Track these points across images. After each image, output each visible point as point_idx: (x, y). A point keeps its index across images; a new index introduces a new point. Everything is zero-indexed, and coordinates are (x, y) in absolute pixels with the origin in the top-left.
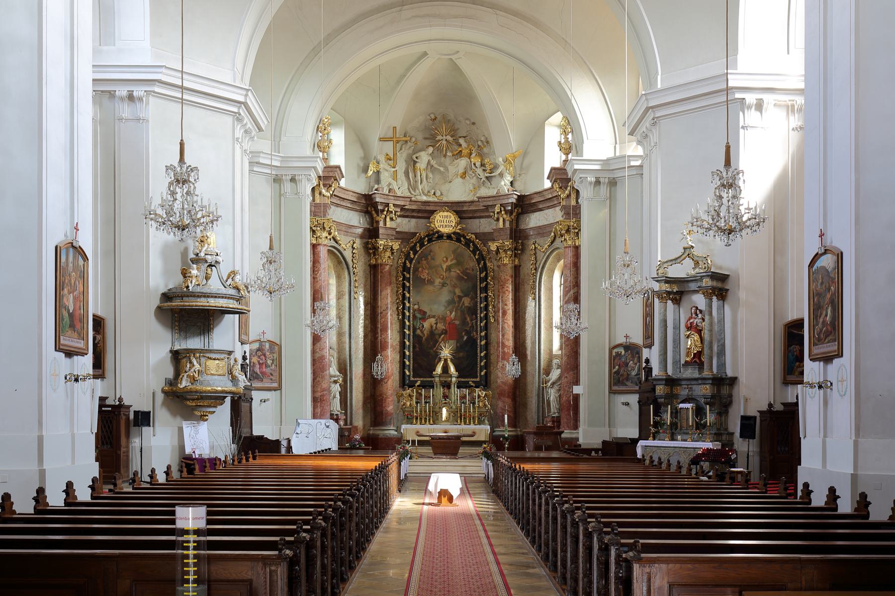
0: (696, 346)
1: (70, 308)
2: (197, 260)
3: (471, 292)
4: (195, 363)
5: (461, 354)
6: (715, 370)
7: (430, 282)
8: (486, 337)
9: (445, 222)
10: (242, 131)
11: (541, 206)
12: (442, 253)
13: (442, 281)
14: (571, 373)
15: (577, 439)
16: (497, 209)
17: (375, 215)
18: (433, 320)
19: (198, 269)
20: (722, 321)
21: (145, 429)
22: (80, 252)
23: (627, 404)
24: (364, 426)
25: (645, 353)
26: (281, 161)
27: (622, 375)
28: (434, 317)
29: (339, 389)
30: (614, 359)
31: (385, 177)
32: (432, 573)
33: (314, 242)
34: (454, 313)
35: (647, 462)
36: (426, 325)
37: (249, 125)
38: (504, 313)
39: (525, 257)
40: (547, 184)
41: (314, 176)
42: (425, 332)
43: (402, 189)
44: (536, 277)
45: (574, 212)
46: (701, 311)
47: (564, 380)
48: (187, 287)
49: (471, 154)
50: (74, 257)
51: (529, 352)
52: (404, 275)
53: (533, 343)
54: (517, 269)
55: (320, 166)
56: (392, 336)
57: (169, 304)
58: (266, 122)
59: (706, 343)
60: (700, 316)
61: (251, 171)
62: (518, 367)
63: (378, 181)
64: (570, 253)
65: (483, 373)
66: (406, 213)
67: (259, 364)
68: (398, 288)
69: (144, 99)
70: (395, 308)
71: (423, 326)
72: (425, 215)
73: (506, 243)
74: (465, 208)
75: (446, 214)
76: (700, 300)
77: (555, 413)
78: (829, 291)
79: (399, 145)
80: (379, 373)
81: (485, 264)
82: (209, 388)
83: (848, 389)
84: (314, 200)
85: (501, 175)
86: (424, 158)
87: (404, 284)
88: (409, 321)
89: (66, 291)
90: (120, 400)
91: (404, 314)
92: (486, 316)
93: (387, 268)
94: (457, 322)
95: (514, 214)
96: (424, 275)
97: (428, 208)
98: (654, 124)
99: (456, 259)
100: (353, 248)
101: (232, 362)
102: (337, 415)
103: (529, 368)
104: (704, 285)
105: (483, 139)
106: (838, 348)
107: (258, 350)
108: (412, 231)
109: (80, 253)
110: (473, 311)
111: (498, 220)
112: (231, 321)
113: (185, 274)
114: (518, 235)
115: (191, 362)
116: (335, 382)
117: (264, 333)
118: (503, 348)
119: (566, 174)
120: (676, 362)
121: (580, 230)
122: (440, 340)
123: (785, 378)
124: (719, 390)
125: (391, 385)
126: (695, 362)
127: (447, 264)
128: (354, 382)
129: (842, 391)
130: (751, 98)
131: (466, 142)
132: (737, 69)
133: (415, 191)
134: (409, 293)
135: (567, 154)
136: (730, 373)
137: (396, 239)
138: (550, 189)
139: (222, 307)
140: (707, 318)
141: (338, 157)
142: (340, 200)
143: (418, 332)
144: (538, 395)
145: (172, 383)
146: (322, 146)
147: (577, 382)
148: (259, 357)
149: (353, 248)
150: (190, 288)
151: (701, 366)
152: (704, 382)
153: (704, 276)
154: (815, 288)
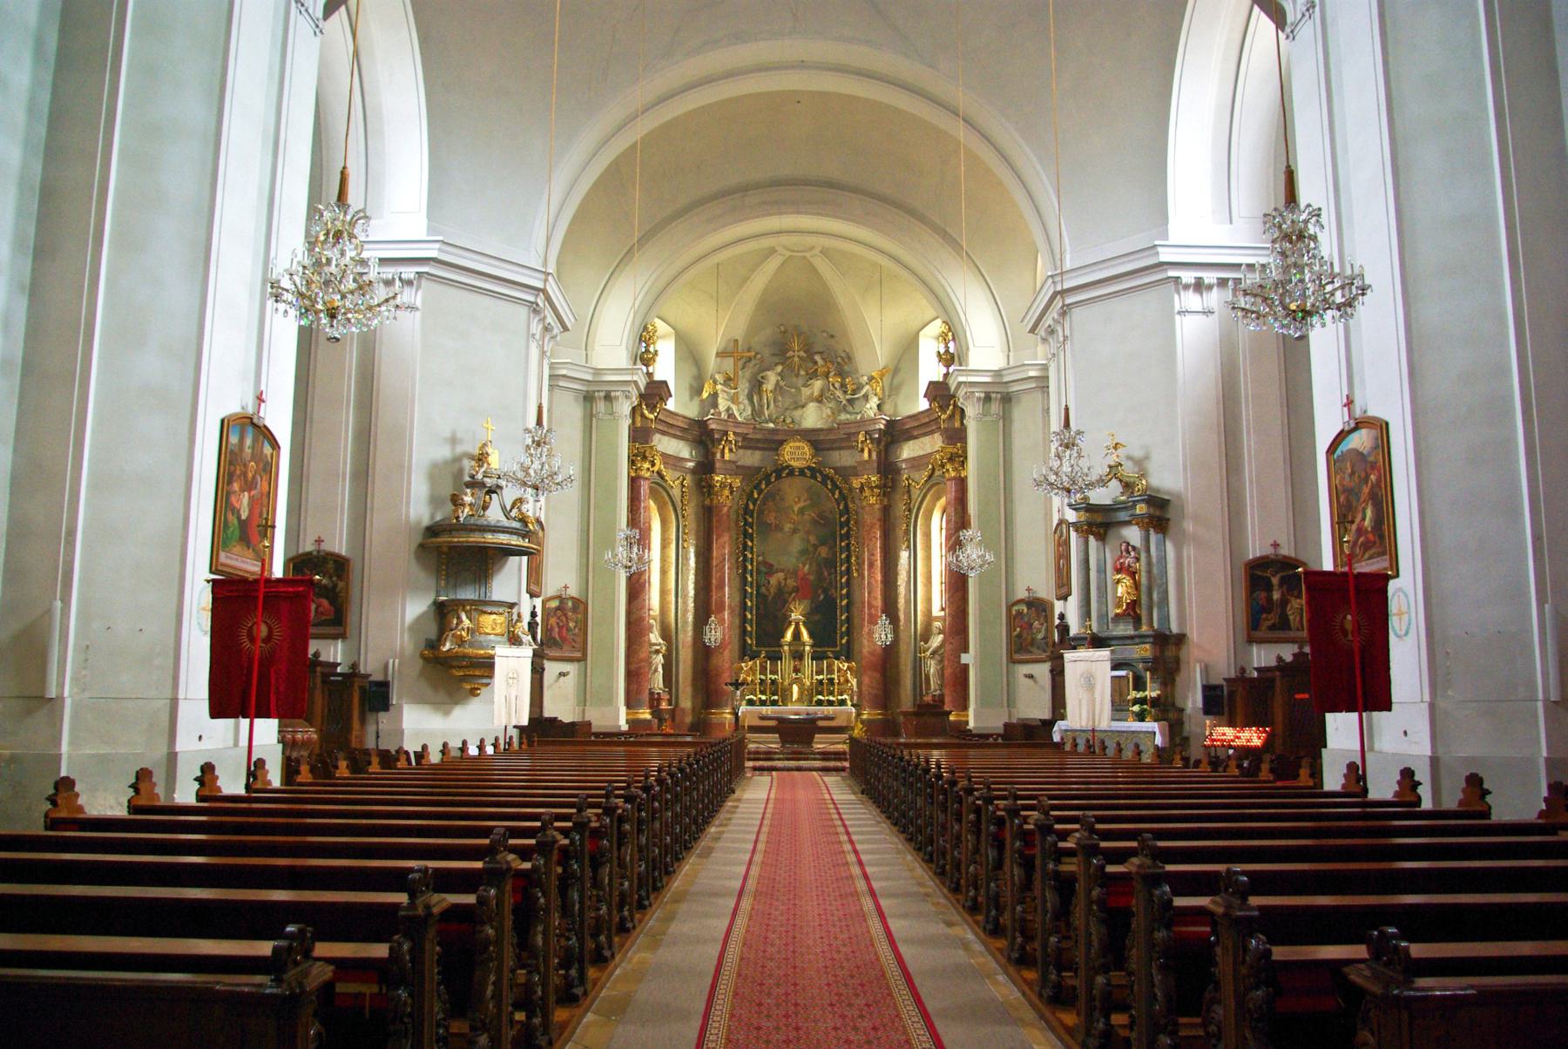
0: (1128, 593)
1: (242, 512)
2: (474, 484)
3: (828, 540)
4: (464, 617)
5: (816, 618)
6: (1156, 625)
7: (779, 528)
8: (848, 595)
9: (796, 454)
10: (541, 326)
11: (916, 433)
12: (794, 495)
13: (792, 526)
14: (958, 638)
15: (967, 723)
16: (861, 438)
17: (710, 446)
18: (781, 575)
19: (473, 495)
20: (1163, 559)
21: (381, 714)
22: (265, 434)
23: (1031, 676)
24: (694, 709)
25: (1058, 607)
26: (594, 374)
27: (1025, 639)
28: (782, 571)
29: (662, 661)
30: (1013, 619)
31: (723, 404)
32: (766, 938)
33: (633, 474)
34: (807, 567)
35: (1068, 747)
36: (773, 581)
37: (549, 320)
38: (871, 565)
39: (897, 496)
40: (923, 404)
41: (635, 393)
42: (772, 590)
43: (742, 412)
44: (910, 519)
45: (957, 436)
46: (1134, 548)
47: (948, 647)
48: (457, 518)
49: (829, 373)
50: (255, 440)
51: (902, 616)
52: (745, 519)
53: (907, 602)
54: (886, 511)
55: (642, 383)
56: (729, 594)
57: (434, 540)
58: (573, 320)
59: (1144, 589)
60: (1133, 554)
61: (551, 387)
62: (889, 628)
63: (715, 405)
64: (951, 487)
65: (844, 641)
66: (747, 443)
67: (559, 627)
68: (738, 534)
69: (415, 282)
70: (733, 561)
71: (769, 582)
72: (773, 446)
73: (873, 479)
74: (822, 437)
75: (798, 444)
76: (1133, 534)
77: (935, 691)
78: (1367, 483)
79: (740, 364)
80: (713, 640)
81: (846, 507)
82: (482, 652)
83: (1413, 626)
84: (634, 422)
85: (866, 397)
86: (772, 379)
87: (746, 531)
88: (751, 576)
89: (236, 486)
90: (354, 666)
91: (745, 568)
92: (848, 570)
93: (725, 509)
94: (812, 577)
95: (883, 443)
96: (771, 519)
97: (776, 438)
98: (1063, 314)
99: (811, 499)
100: (683, 486)
101: (515, 617)
102: (658, 694)
103: (902, 635)
104: (1138, 512)
105: (843, 355)
106: (1391, 565)
107: (558, 608)
108: (756, 465)
109: (265, 437)
110: (831, 563)
111: (862, 450)
112: (517, 566)
113: (456, 501)
114: (888, 469)
115: (459, 618)
116: (657, 652)
117: (566, 587)
118: (869, 609)
119: (948, 389)
120: (1103, 616)
121: (966, 458)
122: (790, 599)
123: (1249, 635)
124: (1162, 651)
125: (725, 661)
126: (1129, 614)
127: (799, 505)
128: (681, 653)
129: (1401, 630)
130: (1188, 276)
131: (823, 359)
132: (1167, 239)
133: (760, 417)
134: (752, 541)
135: (948, 366)
136: (1175, 629)
137: (736, 474)
138: (927, 411)
139: (502, 544)
140: (1143, 556)
141: (665, 368)
142: (670, 427)
143: (763, 590)
144: (914, 668)
145: (433, 645)
146: (646, 359)
147: (966, 650)
148: (559, 618)
149: (683, 486)
150: (462, 519)
151: (1137, 621)
152: (1142, 640)
153: (1138, 501)
154: (1340, 483)
